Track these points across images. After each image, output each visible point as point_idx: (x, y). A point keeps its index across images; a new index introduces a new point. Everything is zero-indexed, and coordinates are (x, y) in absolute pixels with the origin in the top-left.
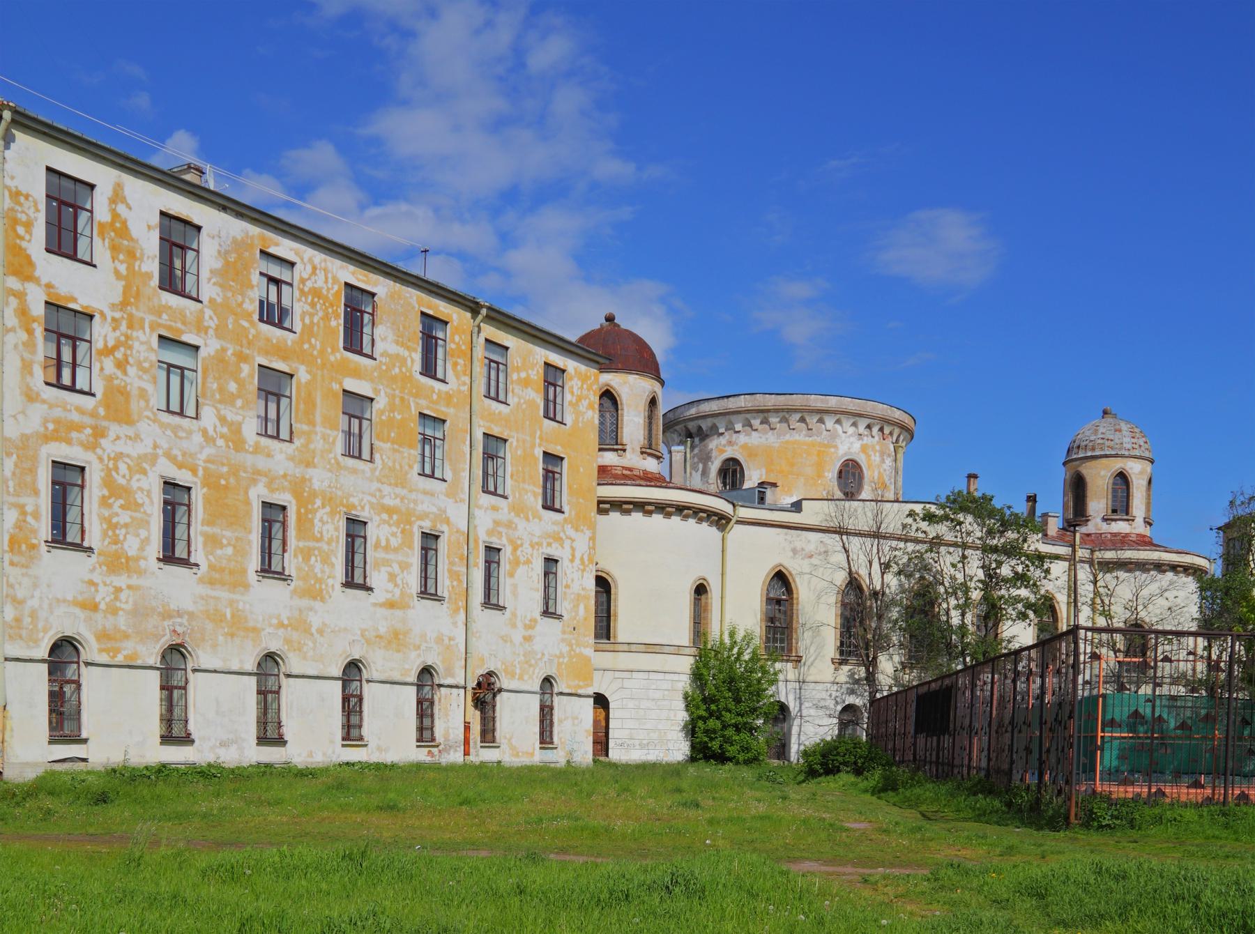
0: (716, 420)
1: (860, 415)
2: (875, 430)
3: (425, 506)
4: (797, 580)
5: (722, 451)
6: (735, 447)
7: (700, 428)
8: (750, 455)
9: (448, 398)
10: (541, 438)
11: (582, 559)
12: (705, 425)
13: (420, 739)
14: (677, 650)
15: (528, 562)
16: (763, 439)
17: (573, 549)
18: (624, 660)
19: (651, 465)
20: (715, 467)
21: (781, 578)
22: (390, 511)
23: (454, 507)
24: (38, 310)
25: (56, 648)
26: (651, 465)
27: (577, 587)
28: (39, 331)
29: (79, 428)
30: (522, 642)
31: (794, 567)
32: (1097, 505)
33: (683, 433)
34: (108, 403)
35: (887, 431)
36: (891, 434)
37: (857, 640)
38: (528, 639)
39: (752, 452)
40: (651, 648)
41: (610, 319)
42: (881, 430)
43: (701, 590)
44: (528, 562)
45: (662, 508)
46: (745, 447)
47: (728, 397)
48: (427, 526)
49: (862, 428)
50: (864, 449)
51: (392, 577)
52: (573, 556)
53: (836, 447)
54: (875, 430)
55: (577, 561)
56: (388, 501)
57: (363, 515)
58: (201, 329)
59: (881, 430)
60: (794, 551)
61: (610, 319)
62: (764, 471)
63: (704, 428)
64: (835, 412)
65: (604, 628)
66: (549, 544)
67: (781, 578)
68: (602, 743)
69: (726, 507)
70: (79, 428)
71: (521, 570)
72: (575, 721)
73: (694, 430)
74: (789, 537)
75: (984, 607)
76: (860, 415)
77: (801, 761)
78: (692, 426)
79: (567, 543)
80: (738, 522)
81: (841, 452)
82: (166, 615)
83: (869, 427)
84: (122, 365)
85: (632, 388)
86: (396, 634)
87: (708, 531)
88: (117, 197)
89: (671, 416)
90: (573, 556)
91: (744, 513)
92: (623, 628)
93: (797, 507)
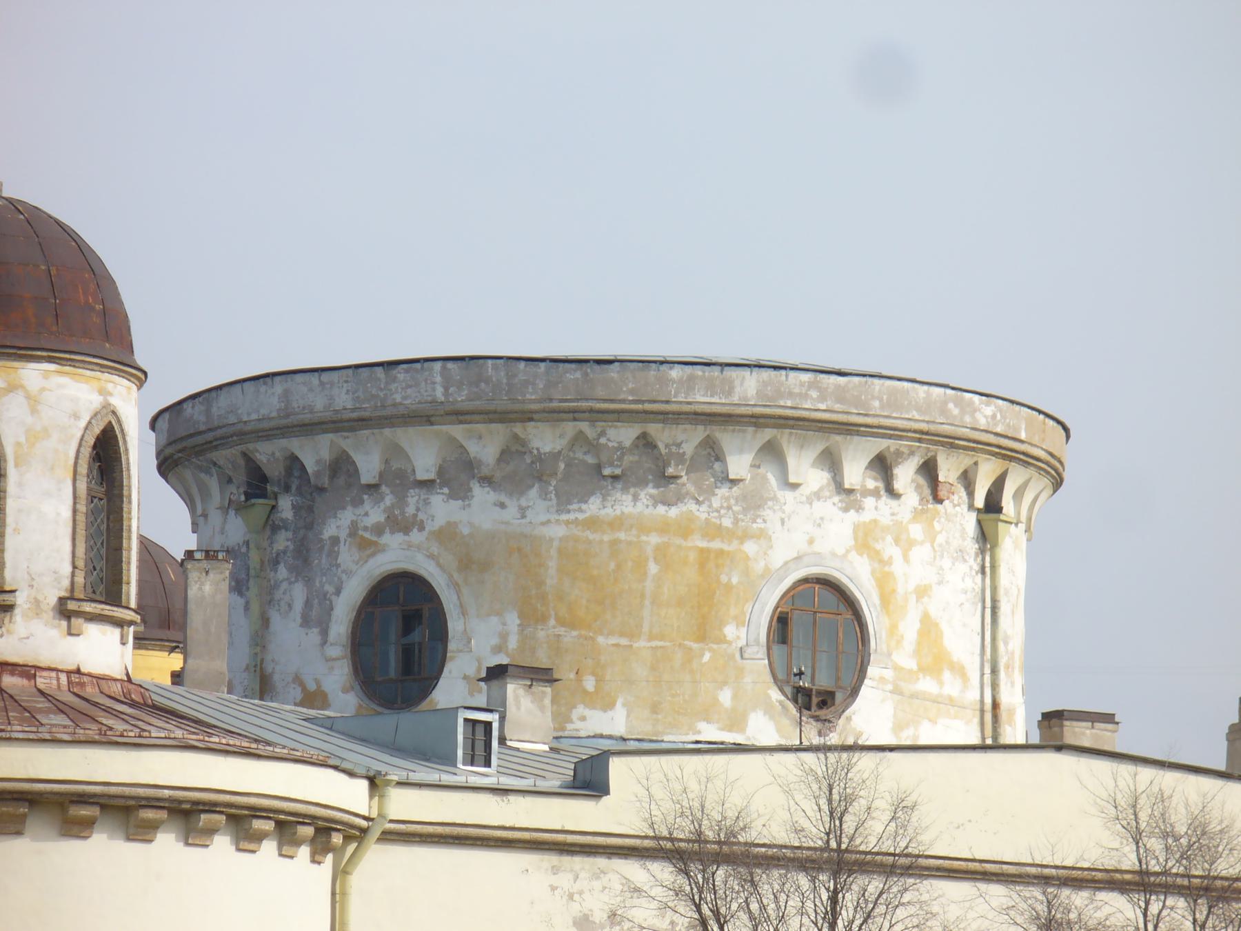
0: (346, 442)
1: (848, 429)
2: (905, 475)
5: (368, 547)
6: (416, 536)
7: (293, 462)
8: (467, 563)
12: (314, 454)
16: (511, 512)
19: (103, 650)
26: (103, 650)
33: (241, 477)
35: (948, 470)
36: (967, 480)
39: (472, 559)
42: (929, 470)
46: (447, 535)
50: (865, 540)
53: (762, 535)
54: (905, 475)
59: (929, 470)
63: (311, 467)
64: (757, 421)
69: (345, 794)
73: (275, 471)
74: (564, 881)
76: (848, 429)
77: (1095, 922)
78: (267, 453)
80: (389, 837)
81: (779, 556)
83: (883, 466)
89: (194, 412)
93: (589, 780)
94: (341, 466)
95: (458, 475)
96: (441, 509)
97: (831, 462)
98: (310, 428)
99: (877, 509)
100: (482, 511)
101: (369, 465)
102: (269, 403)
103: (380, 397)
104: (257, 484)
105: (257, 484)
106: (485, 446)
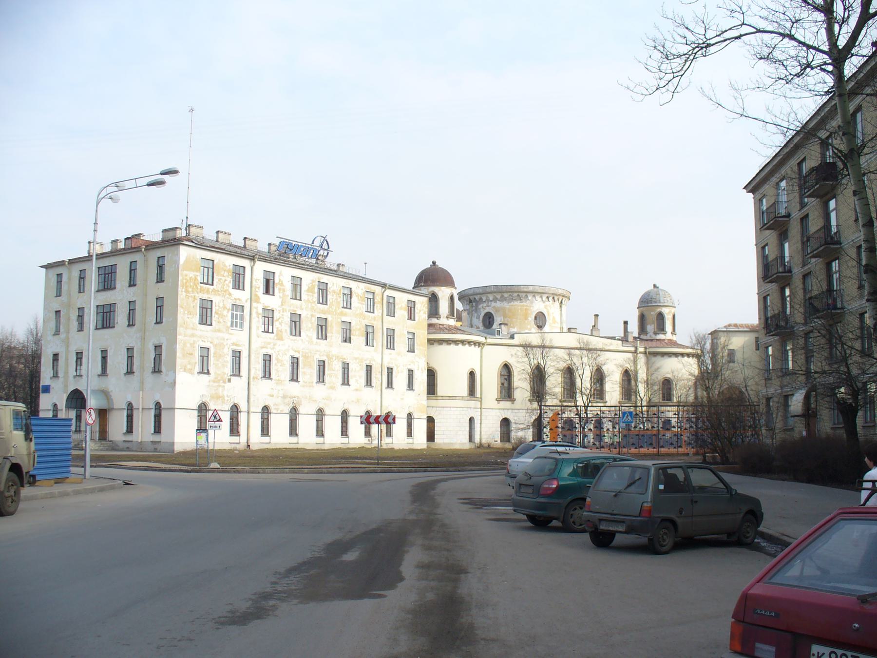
2: (551, 299)
12: (477, 298)
13: (366, 435)
18: (441, 403)
21: (507, 367)
22: (356, 359)
23: (376, 355)
24: (260, 311)
25: (200, 406)
27: (421, 380)
28: (260, 316)
29: (269, 344)
30: (404, 401)
31: (512, 362)
32: (650, 328)
34: (277, 335)
35: (556, 298)
39: (497, 310)
41: (434, 263)
46: (494, 307)
49: (544, 298)
51: (357, 381)
54: (551, 299)
57: (348, 361)
58: (302, 309)
60: (512, 355)
61: (434, 263)
65: (431, 389)
67: (507, 367)
68: (431, 437)
70: (269, 344)
72: (420, 428)
78: (471, 298)
82: (291, 398)
83: (548, 298)
84: (280, 324)
85: (444, 293)
86: (358, 401)
87: (477, 350)
88: (281, 274)
91: (490, 341)
92: (441, 390)
93: (512, 337)
94: (481, 299)
95: (495, 300)
96: (493, 304)
97: (541, 297)
98: (477, 294)
99: (547, 303)
100: (498, 304)
101: (484, 299)
102: (472, 291)
103: (486, 291)
104: (471, 301)
105: (471, 301)
106: (498, 296)
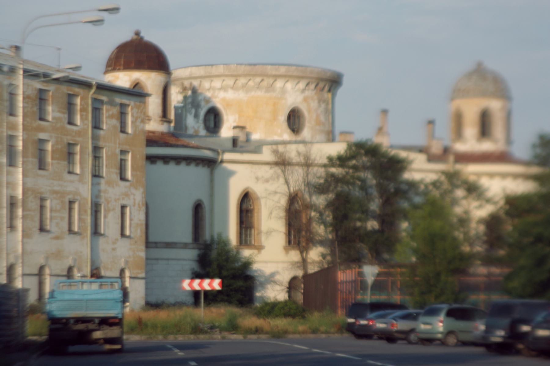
3: (70, 188)
4: (263, 201)
9: (79, 133)
10: (119, 144)
11: (139, 205)
14: (185, 246)
15: (114, 209)
17: (134, 199)
20: (202, 113)
22: (56, 192)
37: (297, 233)
38: (114, 249)
40: (169, 245)
41: (137, 33)
43: (198, 208)
44: (114, 209)
45: (178, 160)
46: (224, 99)
47: (212, 65)
48: (71, 197)
52: (135, 203)
55: (137, 206)
56: (56, 188)
60: (257, 179)
62: (237, 116)
66: (123, 199)
71: (110, 215)
75: (323, 106)
79: (132, 197)
90: (135, 203)
95: (224, 88)
98: (196, 78)
